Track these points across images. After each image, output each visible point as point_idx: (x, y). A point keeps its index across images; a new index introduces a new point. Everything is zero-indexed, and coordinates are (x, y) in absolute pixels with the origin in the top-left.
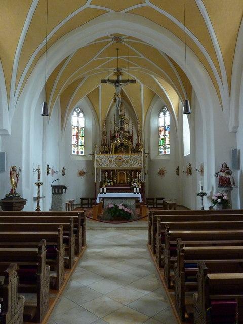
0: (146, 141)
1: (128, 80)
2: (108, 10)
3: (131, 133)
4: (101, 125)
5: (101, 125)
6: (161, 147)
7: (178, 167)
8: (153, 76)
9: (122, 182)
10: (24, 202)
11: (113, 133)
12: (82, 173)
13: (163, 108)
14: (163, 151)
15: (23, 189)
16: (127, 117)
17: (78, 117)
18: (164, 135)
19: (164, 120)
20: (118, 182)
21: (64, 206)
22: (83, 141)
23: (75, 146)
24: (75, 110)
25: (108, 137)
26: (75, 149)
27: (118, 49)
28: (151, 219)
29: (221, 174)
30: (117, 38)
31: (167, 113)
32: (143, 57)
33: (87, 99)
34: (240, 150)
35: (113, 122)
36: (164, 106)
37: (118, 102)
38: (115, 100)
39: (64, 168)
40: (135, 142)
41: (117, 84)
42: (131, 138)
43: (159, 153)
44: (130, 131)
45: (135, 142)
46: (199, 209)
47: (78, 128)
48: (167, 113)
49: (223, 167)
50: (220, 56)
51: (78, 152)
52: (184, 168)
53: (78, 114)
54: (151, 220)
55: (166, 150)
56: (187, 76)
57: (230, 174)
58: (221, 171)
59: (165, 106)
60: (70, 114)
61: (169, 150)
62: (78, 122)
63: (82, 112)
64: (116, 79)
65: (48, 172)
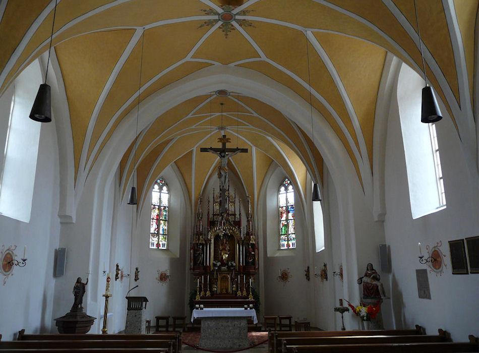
0: (261, 233)
1: (237, 149)
2: (213, 62)
3: (238, 216)
4: (193, 201)
5: (193, 201)
6: (282, 236)
7: (308, 268)
8: (270, 138)
9: (224, 291)
10: (90, 321)
11: (211, 216)
12: (163, 277)
13: (284, 180)
14: (286, 243)
15: (88, 303)
16: (232, 192)
17: (160, 192)
18: (287, 220)
19: (286, 197)
20: (219, 291)
21: (144, 326)
22: (166, 228)
23: (153, 235)
24: (156, 183)
25: (204, 223)
26: (154, 240)
27: (222, 104)
28: (272, 345)
29: (365, 279)
30: (222, 92)
31: (290, 187)
32: (255, 115)
33: (176, 167)
34: (389, 246)
35: (211, 200)
36: (286, 178)
37: (223, 178)
39: (137, 269)
41: (223, 154)
42: (238, 224)
43: (280, 246)
44: (237, 213)
46: (339, 329)
47: (159, 209)
48: (290, 187)
49: (368, 269)
50: (356, 124)
51: (158, 245)
52: (316, 270)
53: (161, 189)
54: (273, 348)
55: (290, 243)
56: (315, 143)
57: (378, 280)
58: (366, 275)
59: (287, 178)
60: (150, 188)
61: (294, 242)
62: (160, 199)
63: (166, 184)
64: (221, 147)
65: (117, 275)
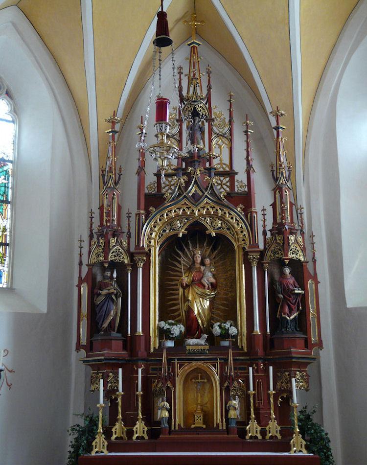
3: (241, 177)
9: (199, 422)
16: (219, 108)
20: (179, 420)
38: (162, 40)
40: (264, 219)
42: (246, 200)
44: (240, 166)
45: (264, 219)
